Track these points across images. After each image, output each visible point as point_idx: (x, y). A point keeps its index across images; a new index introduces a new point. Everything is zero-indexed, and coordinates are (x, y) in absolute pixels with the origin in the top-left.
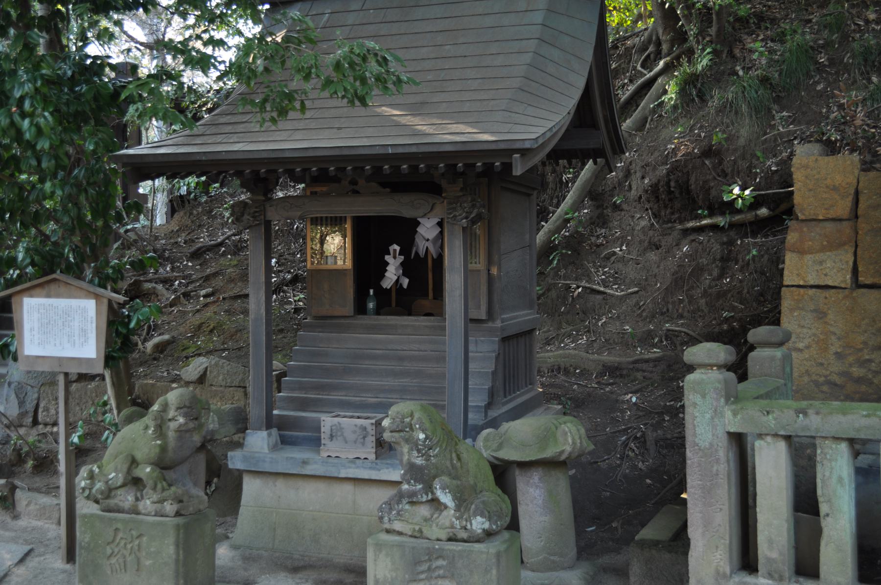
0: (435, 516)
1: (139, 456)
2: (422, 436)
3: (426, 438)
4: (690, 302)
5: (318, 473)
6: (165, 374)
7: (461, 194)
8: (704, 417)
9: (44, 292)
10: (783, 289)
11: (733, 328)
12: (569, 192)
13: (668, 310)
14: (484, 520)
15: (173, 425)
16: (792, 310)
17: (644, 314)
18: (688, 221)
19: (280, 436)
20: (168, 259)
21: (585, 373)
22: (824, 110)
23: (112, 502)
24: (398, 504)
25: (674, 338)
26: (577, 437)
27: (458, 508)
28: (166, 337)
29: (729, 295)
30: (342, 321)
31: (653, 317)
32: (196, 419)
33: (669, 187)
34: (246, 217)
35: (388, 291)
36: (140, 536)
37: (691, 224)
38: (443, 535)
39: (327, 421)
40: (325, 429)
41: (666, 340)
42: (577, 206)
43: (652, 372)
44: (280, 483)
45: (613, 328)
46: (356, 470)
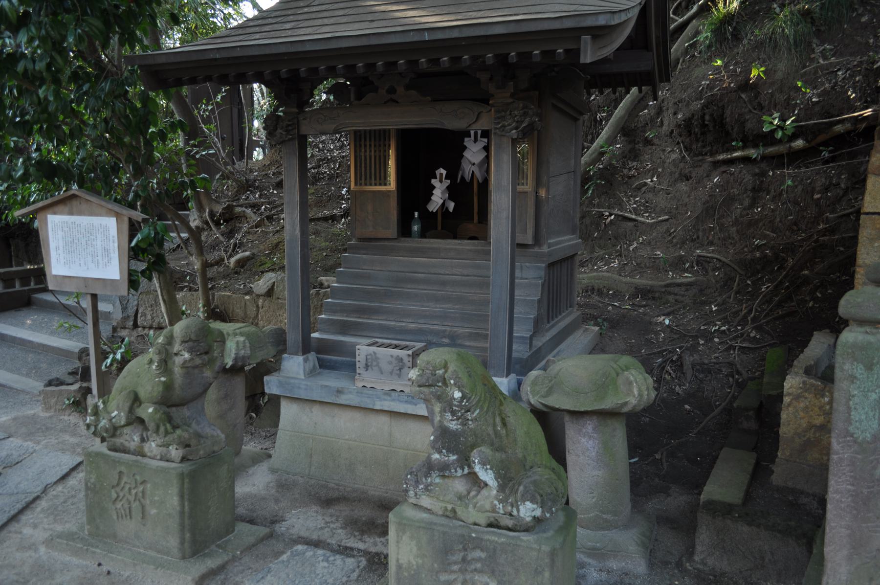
0: (473, 493)
1: (142, 394)
2: (457, 395)
3: (463, 398)
4: (721, 230)
5: (353, 403)
6: (242, 287)
7: (511, 100)
8: (866, 397)
9: (66, 209)
10: (862, 217)
11: (766, 256)
12: (603, 129)
13: (698, 237)
14: (535, 506)
15: (178, 360)
16: (872, 240)
17: (675, 241)
18: (720, 153)
19: (318, 358)
20: (257, 188)
21: (618, 295)
22: (871, 41)
23: (118, 441)
24: (426, 477)
25: (706, 265)
26: (644, 388)
27: (502, 488)
28: (247, 253)
29: (761, 224)
30: (387, 243)
31: (683, 243)
32: (206, 353)
33: (704, 121)
34: (279, 131)
35: (434, 215)
36: (143, 482)
37: (721, 157)
38: (482, 519)
39: (363, 349)
40: (360, 358)
41: (697, 265)
42: (611, 141)
43: (683, 296)
44: (316, 409)
45: (645, 252)
46: (392, 403)
